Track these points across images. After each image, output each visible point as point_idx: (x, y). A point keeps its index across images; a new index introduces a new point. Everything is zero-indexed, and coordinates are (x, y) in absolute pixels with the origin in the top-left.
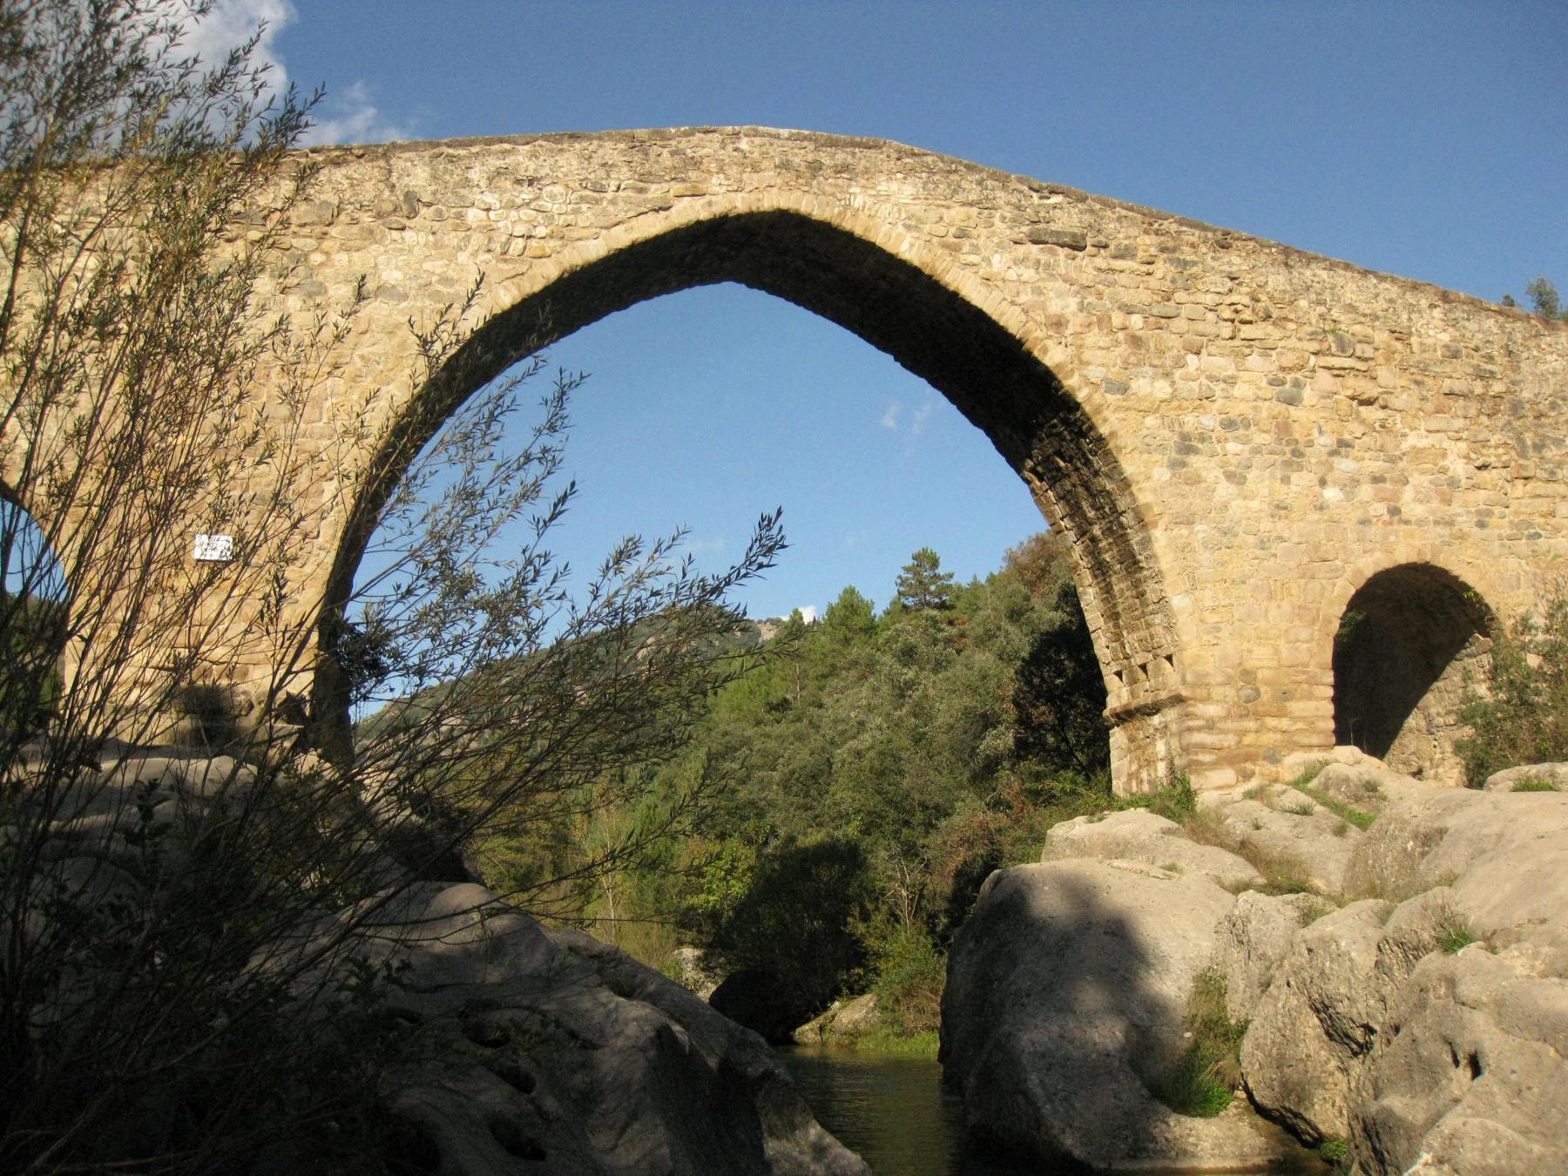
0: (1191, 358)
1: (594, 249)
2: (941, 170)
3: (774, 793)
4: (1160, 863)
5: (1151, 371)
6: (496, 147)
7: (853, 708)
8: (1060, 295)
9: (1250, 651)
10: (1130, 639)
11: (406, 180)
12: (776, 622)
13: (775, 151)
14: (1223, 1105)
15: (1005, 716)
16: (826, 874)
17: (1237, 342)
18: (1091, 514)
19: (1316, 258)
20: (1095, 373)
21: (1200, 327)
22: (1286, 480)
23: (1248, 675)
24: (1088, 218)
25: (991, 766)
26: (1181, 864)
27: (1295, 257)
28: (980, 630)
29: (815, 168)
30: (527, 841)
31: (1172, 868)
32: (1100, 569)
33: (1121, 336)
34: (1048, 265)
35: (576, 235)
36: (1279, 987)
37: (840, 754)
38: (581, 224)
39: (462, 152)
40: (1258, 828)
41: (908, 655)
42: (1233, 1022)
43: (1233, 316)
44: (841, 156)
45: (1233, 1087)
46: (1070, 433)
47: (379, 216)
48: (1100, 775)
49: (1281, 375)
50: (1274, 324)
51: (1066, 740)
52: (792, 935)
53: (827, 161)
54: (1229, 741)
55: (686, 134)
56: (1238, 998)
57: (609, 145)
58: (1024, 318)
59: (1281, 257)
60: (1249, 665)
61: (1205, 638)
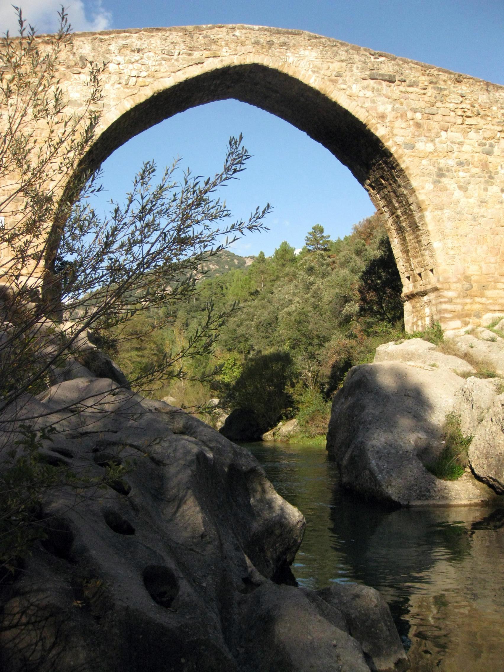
0: (443, 133)
1: (168, 82)
2: (329, 45)
3: (253, 331)
4: (428, 363)
5: (425, 139)
6: (122, 35)
7: (287, 294)
8: (384, 104)
9: (468, 267)
10: (413, 261)
11: (80, 51)
12: (252, 258)
13: (252, 37)
14: (460, 475)
15: (354, 297)
16: (275, 367)
17: (464, 126)
18: (397, 205)
19: (501, 87)
20: (399, 140)
21: (447, 119)
22: (486, 190)
23: (467, 278)
24: (397, 68)
25: (348, 319)
26: (438, 363)
27: (491, 87)
28: (343, 259)
29: (271, 44)
30: (145, 352)
31: (434, 365)
32: (400, 230)
33: (411, 122)
34: (378, 90)
35: (160, 75)
36: (487, 422)
37: (281, 314)
38: (162, 70)
39: (106, 37)
40: (472, 347)
41: (311, 270)
42: (464, 436)
43: (463, 114)
44: (283, 39)
45: (465, 467)
46: (388, 167)
47: (68, 67)
48: (398, 323)
49: (484, 141)
50: (481, 117)
51: (382, 307)
52: (259, 396)
53: (276, 41)
54: (459, 308)
55: (210, 28)
56: (467, 425)
57: (174, 33)
58: (367, 114)
59: (485, 87)
60: (468, 273)
61: (449, 261)
